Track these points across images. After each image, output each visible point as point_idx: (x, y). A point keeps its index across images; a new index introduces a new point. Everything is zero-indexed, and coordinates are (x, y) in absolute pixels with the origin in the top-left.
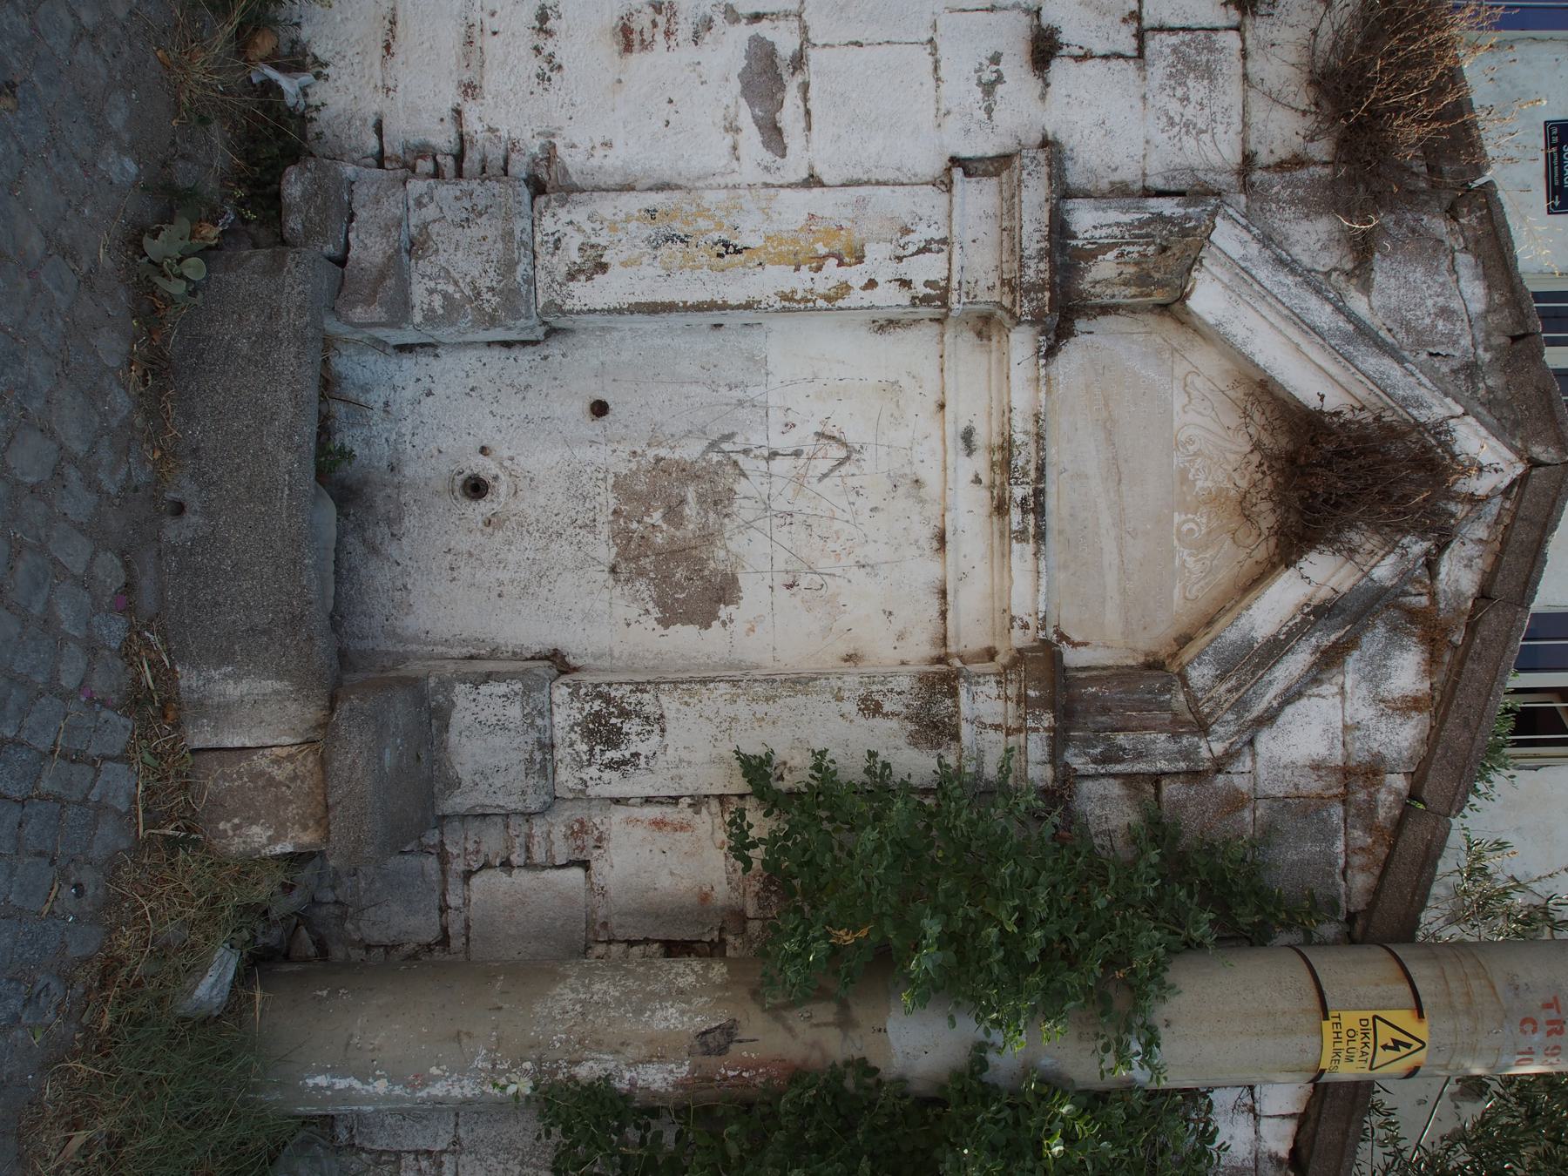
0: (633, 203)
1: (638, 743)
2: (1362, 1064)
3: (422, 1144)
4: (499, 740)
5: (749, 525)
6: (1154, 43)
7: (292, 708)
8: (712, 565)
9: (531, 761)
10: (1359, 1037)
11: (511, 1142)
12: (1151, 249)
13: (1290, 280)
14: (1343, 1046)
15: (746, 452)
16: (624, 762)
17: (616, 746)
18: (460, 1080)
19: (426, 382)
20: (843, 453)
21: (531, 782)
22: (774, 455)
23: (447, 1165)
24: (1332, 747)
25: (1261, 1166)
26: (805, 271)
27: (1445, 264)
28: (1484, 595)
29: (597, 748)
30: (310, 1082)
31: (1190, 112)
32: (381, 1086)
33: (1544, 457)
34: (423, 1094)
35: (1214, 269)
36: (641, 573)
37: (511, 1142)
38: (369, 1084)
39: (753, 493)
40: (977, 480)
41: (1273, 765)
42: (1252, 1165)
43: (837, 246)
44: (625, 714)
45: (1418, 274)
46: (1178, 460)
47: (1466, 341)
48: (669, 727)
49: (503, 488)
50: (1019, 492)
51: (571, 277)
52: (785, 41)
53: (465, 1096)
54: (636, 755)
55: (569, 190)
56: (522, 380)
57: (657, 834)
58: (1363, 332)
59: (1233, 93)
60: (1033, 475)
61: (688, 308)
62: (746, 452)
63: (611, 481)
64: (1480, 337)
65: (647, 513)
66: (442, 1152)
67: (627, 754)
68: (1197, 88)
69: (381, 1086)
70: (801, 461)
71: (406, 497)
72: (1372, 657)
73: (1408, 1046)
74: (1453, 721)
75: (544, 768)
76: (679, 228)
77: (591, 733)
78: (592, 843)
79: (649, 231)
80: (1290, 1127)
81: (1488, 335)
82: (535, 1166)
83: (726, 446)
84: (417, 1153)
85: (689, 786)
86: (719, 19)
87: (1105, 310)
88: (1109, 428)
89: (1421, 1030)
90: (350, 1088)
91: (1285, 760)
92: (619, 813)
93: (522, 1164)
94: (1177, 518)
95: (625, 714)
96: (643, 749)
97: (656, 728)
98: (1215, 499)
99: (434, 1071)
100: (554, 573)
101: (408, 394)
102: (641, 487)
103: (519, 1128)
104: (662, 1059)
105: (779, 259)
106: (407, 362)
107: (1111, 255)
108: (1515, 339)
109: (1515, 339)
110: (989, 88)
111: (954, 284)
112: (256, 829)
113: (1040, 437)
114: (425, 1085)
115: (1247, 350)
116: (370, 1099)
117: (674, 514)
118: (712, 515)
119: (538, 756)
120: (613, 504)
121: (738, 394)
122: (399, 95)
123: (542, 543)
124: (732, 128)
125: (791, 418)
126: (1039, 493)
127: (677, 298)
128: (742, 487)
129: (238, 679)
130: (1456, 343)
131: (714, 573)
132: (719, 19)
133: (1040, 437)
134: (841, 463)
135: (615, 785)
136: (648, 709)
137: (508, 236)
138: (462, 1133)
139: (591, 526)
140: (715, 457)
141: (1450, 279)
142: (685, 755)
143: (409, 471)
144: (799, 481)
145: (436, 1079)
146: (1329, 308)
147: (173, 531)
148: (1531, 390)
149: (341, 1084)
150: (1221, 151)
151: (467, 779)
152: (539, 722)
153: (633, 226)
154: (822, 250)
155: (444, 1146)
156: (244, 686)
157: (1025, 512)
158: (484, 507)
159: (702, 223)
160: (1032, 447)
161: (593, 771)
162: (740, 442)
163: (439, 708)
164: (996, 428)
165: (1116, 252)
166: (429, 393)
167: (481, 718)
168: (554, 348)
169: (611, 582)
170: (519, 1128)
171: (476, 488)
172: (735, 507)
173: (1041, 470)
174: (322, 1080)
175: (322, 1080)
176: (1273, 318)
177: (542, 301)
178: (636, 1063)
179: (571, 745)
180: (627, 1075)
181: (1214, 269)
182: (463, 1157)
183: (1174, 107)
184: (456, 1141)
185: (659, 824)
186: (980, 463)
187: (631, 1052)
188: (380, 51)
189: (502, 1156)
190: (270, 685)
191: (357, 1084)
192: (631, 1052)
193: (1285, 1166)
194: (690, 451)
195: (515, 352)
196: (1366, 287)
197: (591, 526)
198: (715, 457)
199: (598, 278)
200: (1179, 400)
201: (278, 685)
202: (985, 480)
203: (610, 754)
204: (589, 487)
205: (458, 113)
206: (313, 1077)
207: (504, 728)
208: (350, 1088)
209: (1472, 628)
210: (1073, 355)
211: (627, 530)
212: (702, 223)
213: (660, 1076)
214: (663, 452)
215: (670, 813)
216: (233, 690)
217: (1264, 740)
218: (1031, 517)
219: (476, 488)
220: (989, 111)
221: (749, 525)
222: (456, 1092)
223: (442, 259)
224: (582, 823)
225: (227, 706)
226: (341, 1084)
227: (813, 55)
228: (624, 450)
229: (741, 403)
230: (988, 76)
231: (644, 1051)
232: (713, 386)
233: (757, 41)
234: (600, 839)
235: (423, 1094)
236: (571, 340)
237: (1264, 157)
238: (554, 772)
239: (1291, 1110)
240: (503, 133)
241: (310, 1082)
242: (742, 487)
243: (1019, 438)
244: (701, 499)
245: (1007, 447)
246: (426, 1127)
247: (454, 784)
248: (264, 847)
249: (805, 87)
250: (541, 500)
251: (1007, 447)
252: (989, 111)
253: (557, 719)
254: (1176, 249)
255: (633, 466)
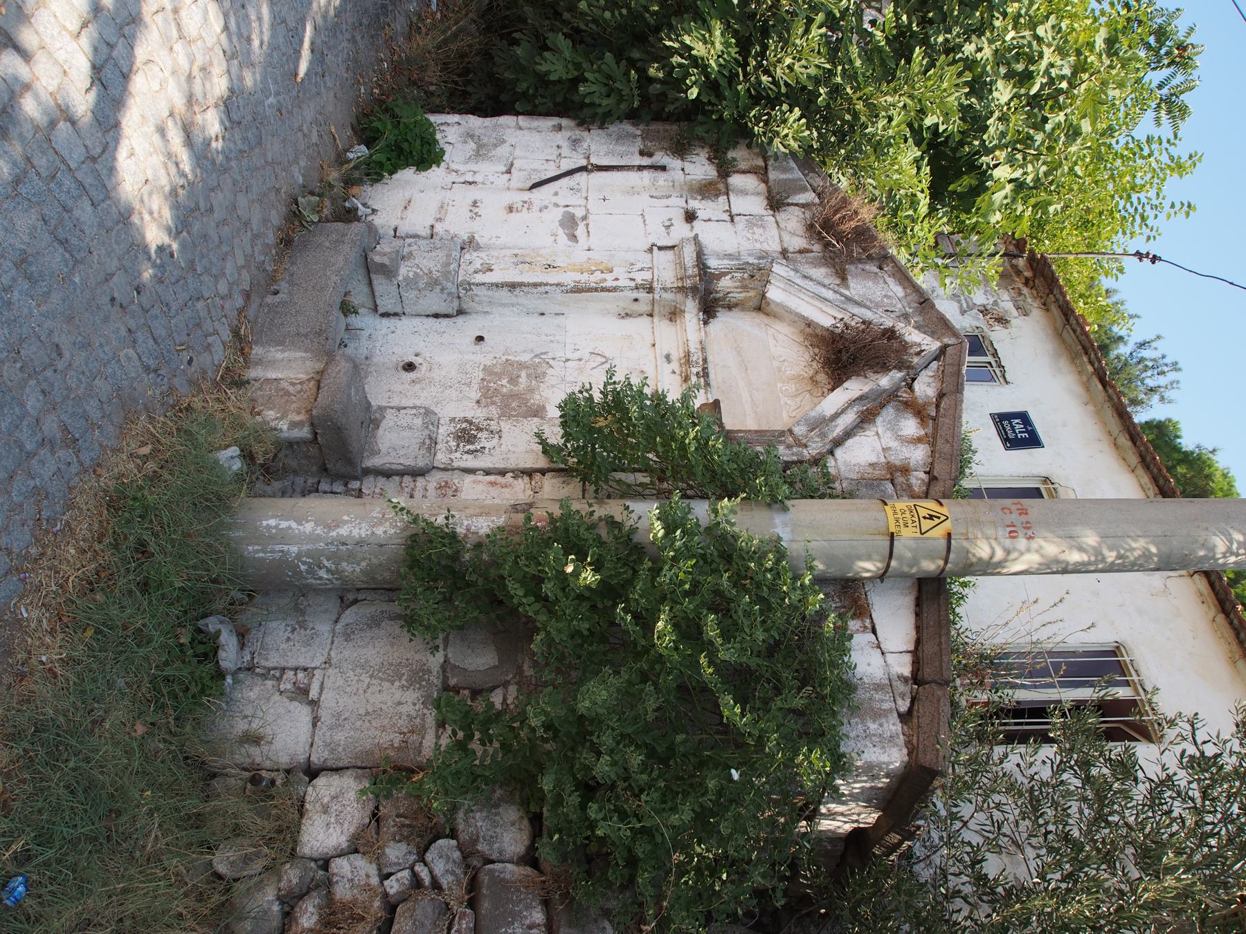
0: (508, 252)
1: (484, 440)
2: (914, 529)
3: (302, 662)
4: (406, 434)
5: (553, 386)
6: (737, 219)
7: (308, 363)
8: (532, 401)
9: (424, 443)
10: (908, 512)
11: (367, 661)
12: (746, 275)
13: (811, 283)
14: (899, 516)
15: (553, 359)
16: (476, 451)
17: (473, 443)
18: (360, 523)
19: (393, 328)
20: (604, 360)
21: (421, 452)
22: (568, 360)
23: (316, 677)
24: (878, 458)
25: (894, 683)
26: (585, 274)
27: (882, 281)
28: (941, 396)
29: (462, 444)
30: (265, 523)
31: (756, 237)
32: (308, 527)
33: (950, 342)
34: (334, 534)
35: (777, 284)
36: (493, 403)
37: (367, 661)
38: (302, 525)
39: (556, 374)
40: (674, 372)
41: (846, 464)
42: (887, 682)
43: (601, 268)
44: (479, 429)
45: (870, 283)
46: (776, 364)
47: (899, 306)
48: (504, 436)
49: (424, 368)
50: (694, 370)
51: (476, 272)
52: (579, 213)
53: (360, 536)
54: (484, 448)
55: (478, 248)
56: (442, 330)
57: (491, 489)
58: (849, 299)
59: (775, 232)
60: (701, 363)
61: (529, 285)
62: (553, 359)
63: (482, 367)
64: (906, 305)
65: (500, 380)
66: (315, 668)
67: (478, 448)
68: (758, 231)
69: (308, 527)
70: (582, 362)
71: (372, 369)
72: (890, 421)
73: (939, 518)
74: (940, 442)
75: (429, 449)
76: (528, 260)
77: (459, 437)
78: (451, 493)
79: (515, 260)
80: (908, 659)
81: (909, 304)
82: (381, 679)
83: (543, 356)
84: (296, 669)
85: (512, 464)
86: (551, 206)
87: (730, 307)
88: (738, 351)
89: (944, 510)
90: (290, 528)
91: (853, 462)
92: (469, 478)
93: (371, 677)
94: (779, 385)
95: (479, 429)
96: (488, 445)
97: (497, 436)
98: (798, 378)
99: (345, 518)
100: (445, 402)
101: (383, 332)
102: (498, 370)
103: (373, 652)
104: (488, 514)
105: (574, 270)
106: (385, 321)
107: (728, 277)
108: (921, 304)
109: (921, 304)
110: (668, 227)
111: (655, 279)
112: (271, 412)
113: (703, 349)
114: (337, 526)
115: (798, 311)
116: (299, 539)
117: (514, 380)
118: (534, 382)
119: (428, 442)
120: (481, 376)
121: (552, 338)
122: (407, 221)
123: (441, 390)
124: (555, 235)
125: (577, 347)
126: (705, 369)
127: (526, 280)
128: (550, 371)
129: (283, 351)
130: (895, 306)
131: (534, 404)
132: (551, 206)
133: (703, 349)
134: (603, 363)
135: (470, 462)
136: (492, 428)
137: (449, 256)
138: (333, 654)
139: (469, 385)
140: (537, 360)
141: (886, 286)
142: (512, 449)
143: (375, 360)
144: (581, 370)
145: (346, 522)
146: (831, 292)
147: (270, 299)
148: (935, 319)
149: (284, 524)
150: (774, 247)
151: (384, 450)
152: (431, 427)
153: (507, 259)
154: (594, 268)
155: (318, 664)
156: (286, 354)
157: (698, 377)
158: (412, 375)
159: (538, 259)
160: (700, 354)
161: (458, 455)
162: (551, 355)
163: (376, 419)
164: (681, 350)
165: (729, 276)
166: (393, 332)
167: (399, 423)
168: (460, 320)
169: (476, 407)
170: (373, 652)
171: (410, 367)
172: (546, 379)
173: (705, 360)
174: (272, 522)
175: (272, 522)
176: (807, 299)
177: (460, 279)
178: (472, 516)
179: (447, 442)
180: (466, 523)
181: (777, 284)
182: (330, 670)
183: (749, 235)
184: (328, 662)
185: (493, 484)
186: (675, 365)
187: (469, 511)
188: (402, 208)
189: (358, 671)
190: (299, 354)
191: (294, 525)
192: (469, 511)
193: (910, 682)
194: (525, 358)
195: (440, 320)
196: (847, 287)
197: (469, 385)
198: (537, 360)
199: (489, 273)
200: (772, 342)
201: (303, 355)
202: (678, 372)
203: (468, 447)
204: (470, 370)
205: (432, 227)
206: (267, 520)
207: (411, 428)
208: (290, 528)
209: (938, 406)
210: (716, 325)
211: (487, 386)
212: (538, 259)
213: (486, 524)
214: (509, 358)
215: (499, 479)
216: (279, 356)
217: (839, 452)
218: (702, 380)
219: (410, 367)
220: (668, 234)
221: (553, 386)
222: (356, 533)
223: (416, 261)
224: (447, 483)
225: (274, 361)
226: (284, 524)
227: (590, 216)
228: (490, 356)
229: (552, 341)
230: (667, 223)
231: (478, 510)
232: (539, 335)
233: (568, 213)
234: (456, 491)
235: (334, 534)
236: (468, 317)
237: (791, 249)
238: (435, 454)
239: (905, 648)
240: (452, 232)
241: (265, 523)
242: (550, 371)
243: (692, 350)
244: (528, 376)
245: (688, 355)
246: (309, 651)
247: (376, 452)
248: (272, 420)
249: (587, 225)
250: (443, 373)
251: (688, 355)
252: (668, 234)
253: (440, 431)
254: (757, 276)
255: (495, 362)
